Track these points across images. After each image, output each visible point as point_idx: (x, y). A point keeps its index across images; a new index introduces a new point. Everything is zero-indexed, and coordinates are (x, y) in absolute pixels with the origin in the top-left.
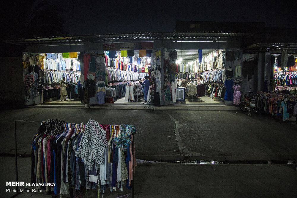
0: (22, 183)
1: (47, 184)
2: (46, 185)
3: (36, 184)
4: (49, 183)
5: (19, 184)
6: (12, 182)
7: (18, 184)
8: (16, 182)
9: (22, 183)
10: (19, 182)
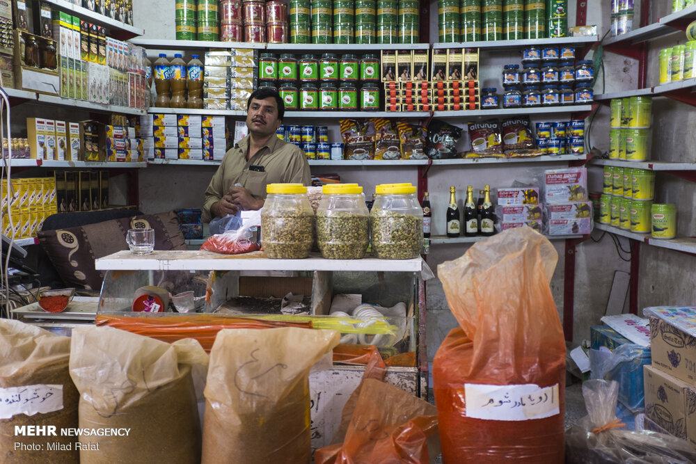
0: (52, 429)
1: (110, 430)
2: (71, 433)
3: (83, 432)
4: (115, 430)
5: (44, 430)
6: (29, 427)
7: (41, 430)
8: (38, 427)
9: (52, 429)
10: (44, 427)
